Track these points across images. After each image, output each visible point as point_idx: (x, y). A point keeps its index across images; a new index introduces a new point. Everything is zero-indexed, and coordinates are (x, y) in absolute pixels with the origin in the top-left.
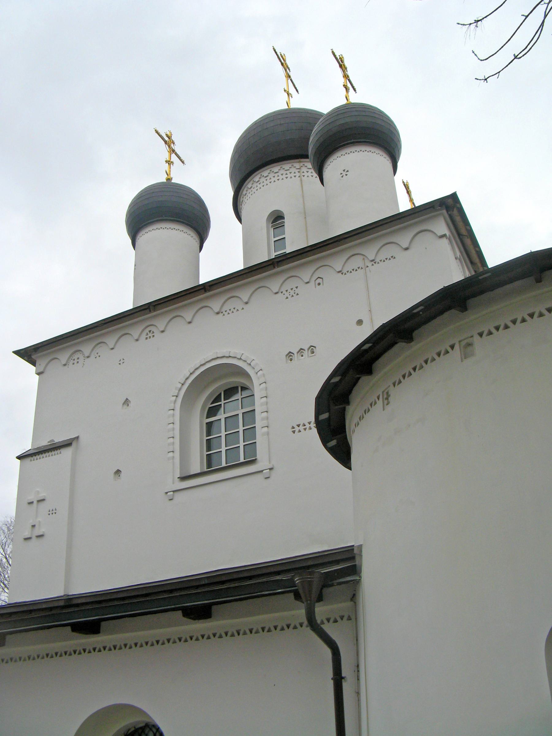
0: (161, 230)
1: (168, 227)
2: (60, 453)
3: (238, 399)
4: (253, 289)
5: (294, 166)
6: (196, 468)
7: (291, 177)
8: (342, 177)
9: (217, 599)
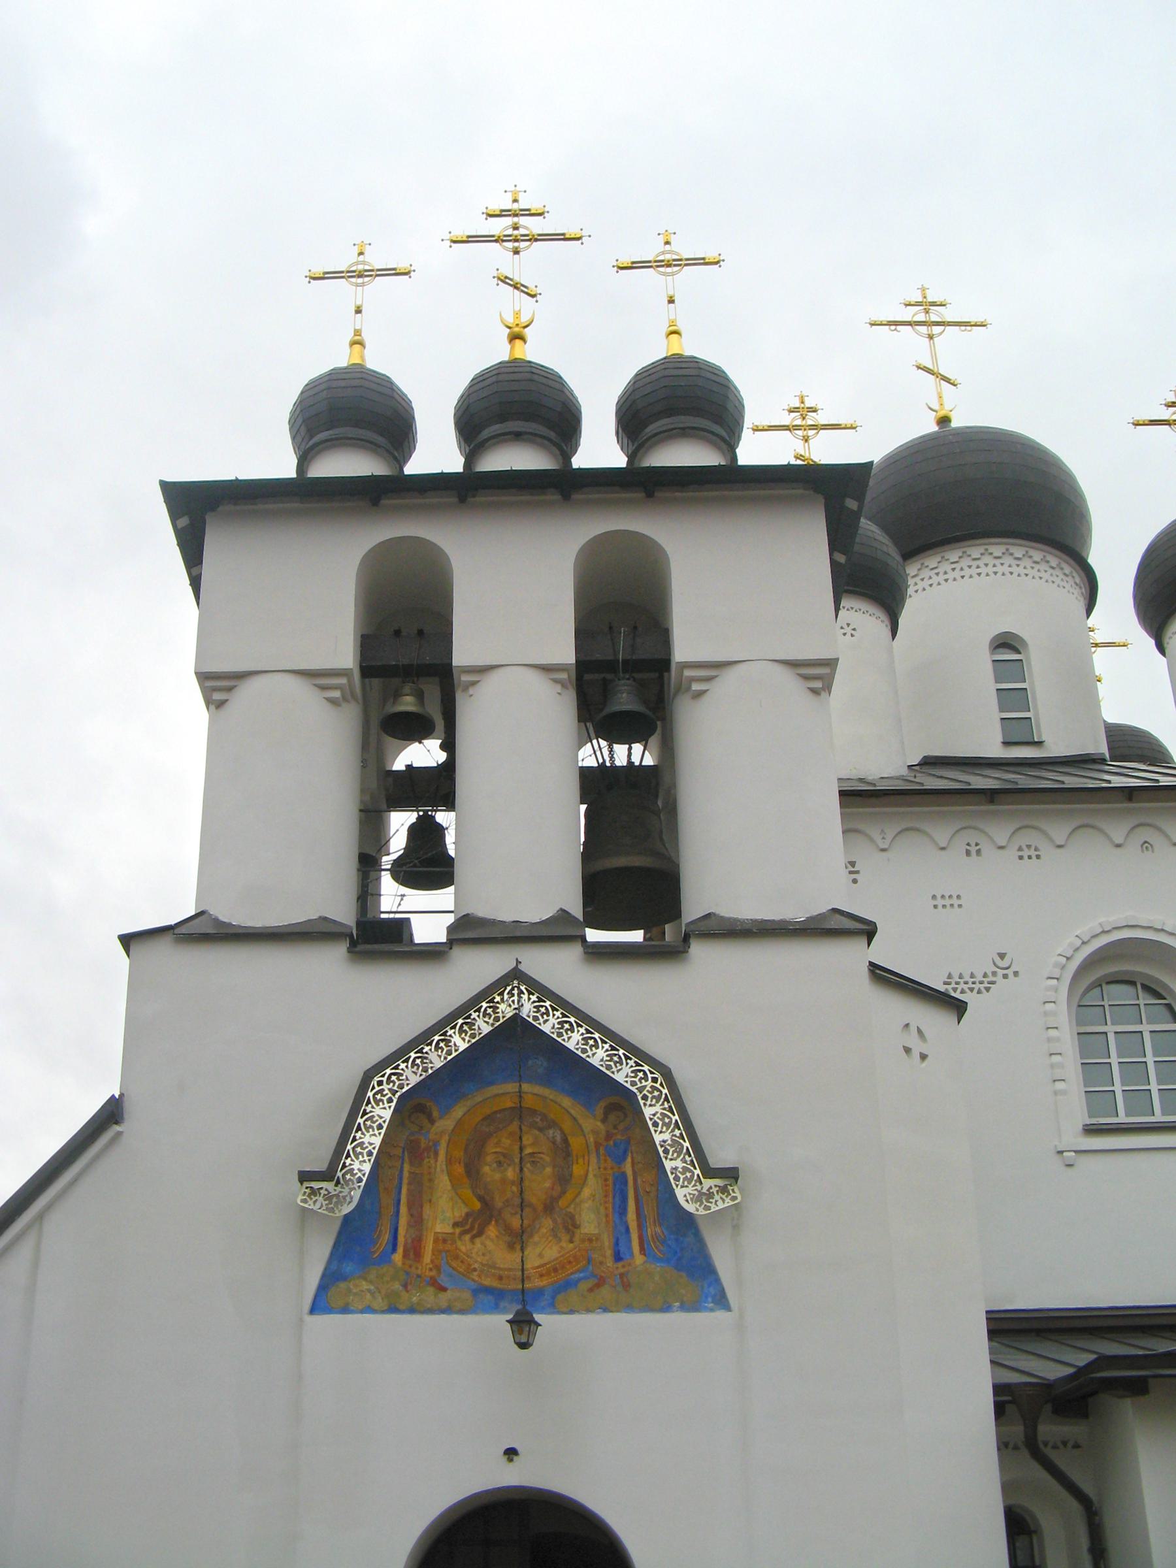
5: (968, 553)
7: (924, 589)
8: (854, 629)
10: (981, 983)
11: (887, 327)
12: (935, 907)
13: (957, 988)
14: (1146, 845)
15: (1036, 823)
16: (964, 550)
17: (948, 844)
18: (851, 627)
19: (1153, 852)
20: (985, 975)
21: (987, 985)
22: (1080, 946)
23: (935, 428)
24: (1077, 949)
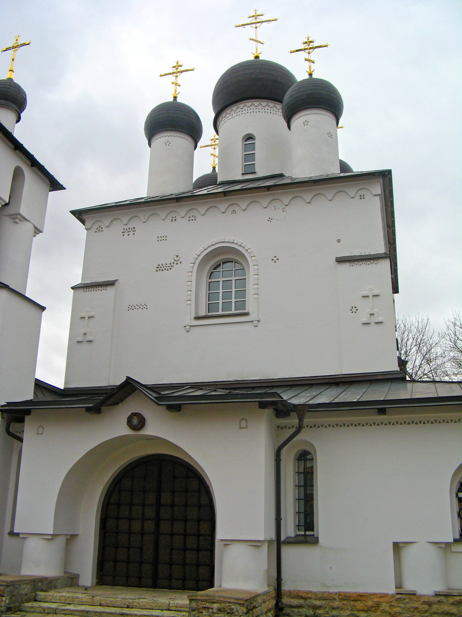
0: (300, 118)
1: (320, 113)
2: (106, 290)
3: (233, 270)
4: (250, 201)
6: (203, 312)
8: (166, 145)
9: (229, 399)
10: (169, 266)
11: (241, 27)
12: (166, 240)
13: (160, 269)
14: (234, 212)
15: (300, 195)
16: (238, 106)
17: (333, 198)
18: (169, 142)
19: (236, 214)
20: (171, 264)
21: (170, 267)
22: (204, 251)
23: (253, 59)
24: (202, 252)
